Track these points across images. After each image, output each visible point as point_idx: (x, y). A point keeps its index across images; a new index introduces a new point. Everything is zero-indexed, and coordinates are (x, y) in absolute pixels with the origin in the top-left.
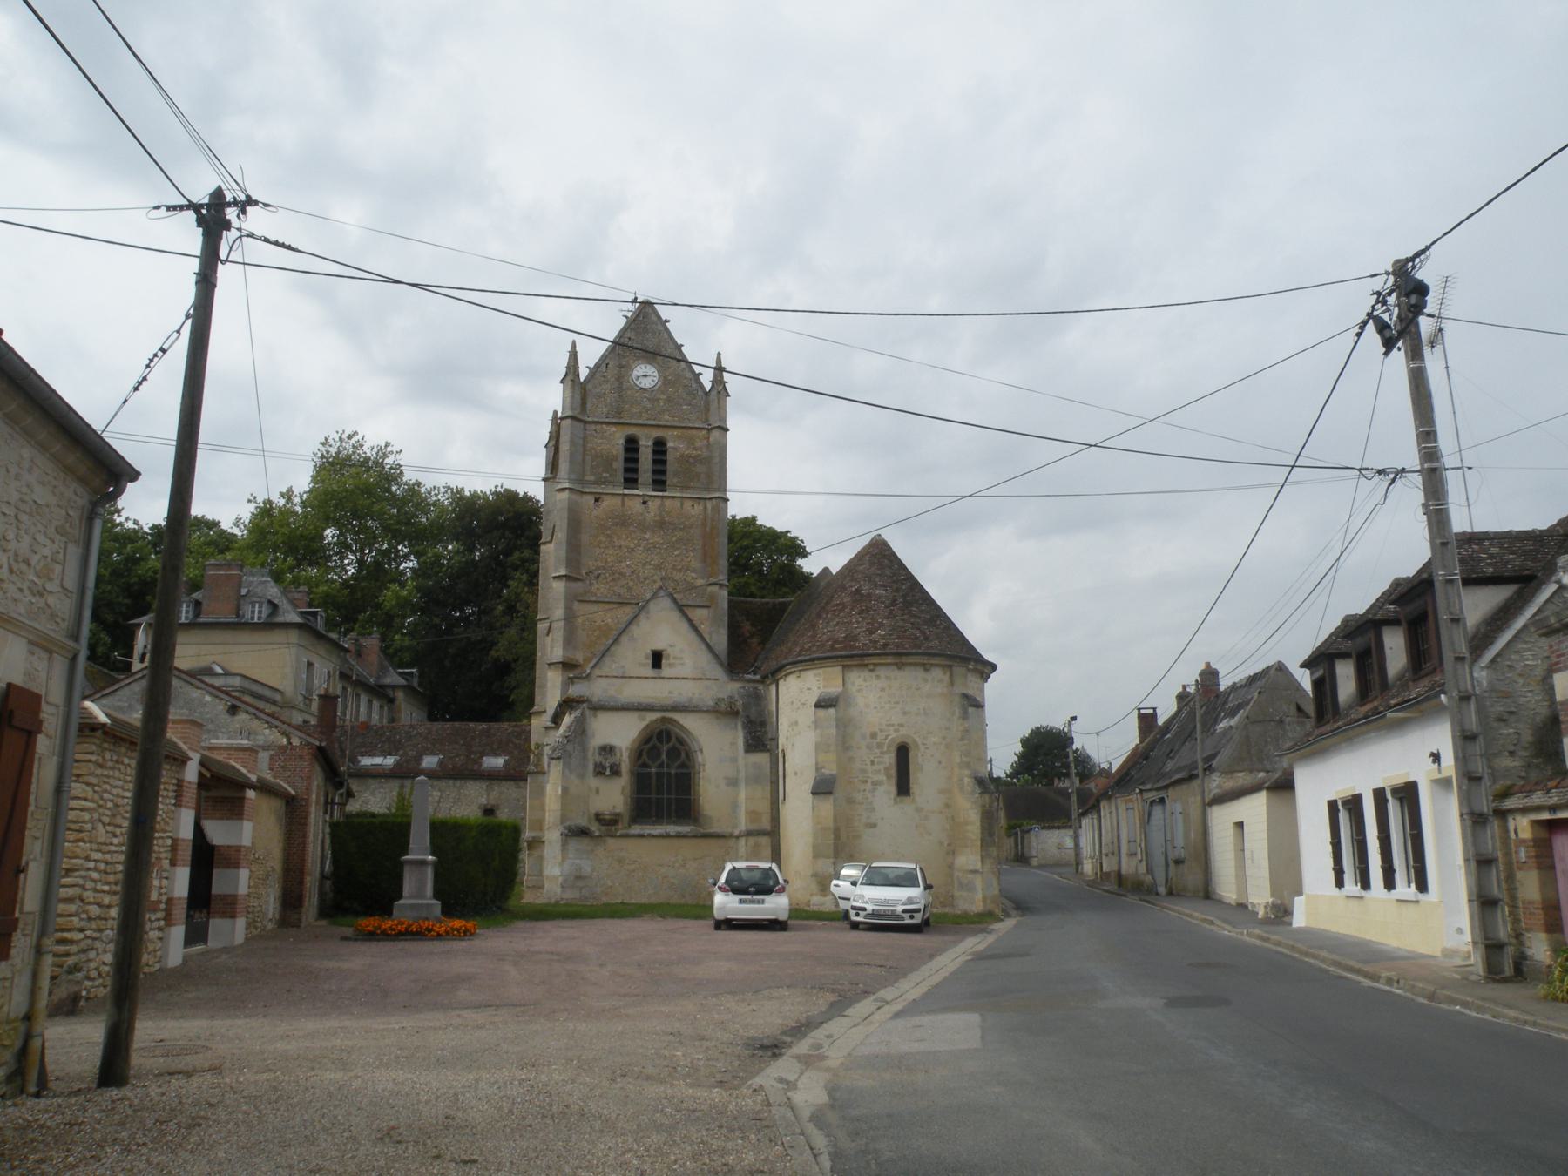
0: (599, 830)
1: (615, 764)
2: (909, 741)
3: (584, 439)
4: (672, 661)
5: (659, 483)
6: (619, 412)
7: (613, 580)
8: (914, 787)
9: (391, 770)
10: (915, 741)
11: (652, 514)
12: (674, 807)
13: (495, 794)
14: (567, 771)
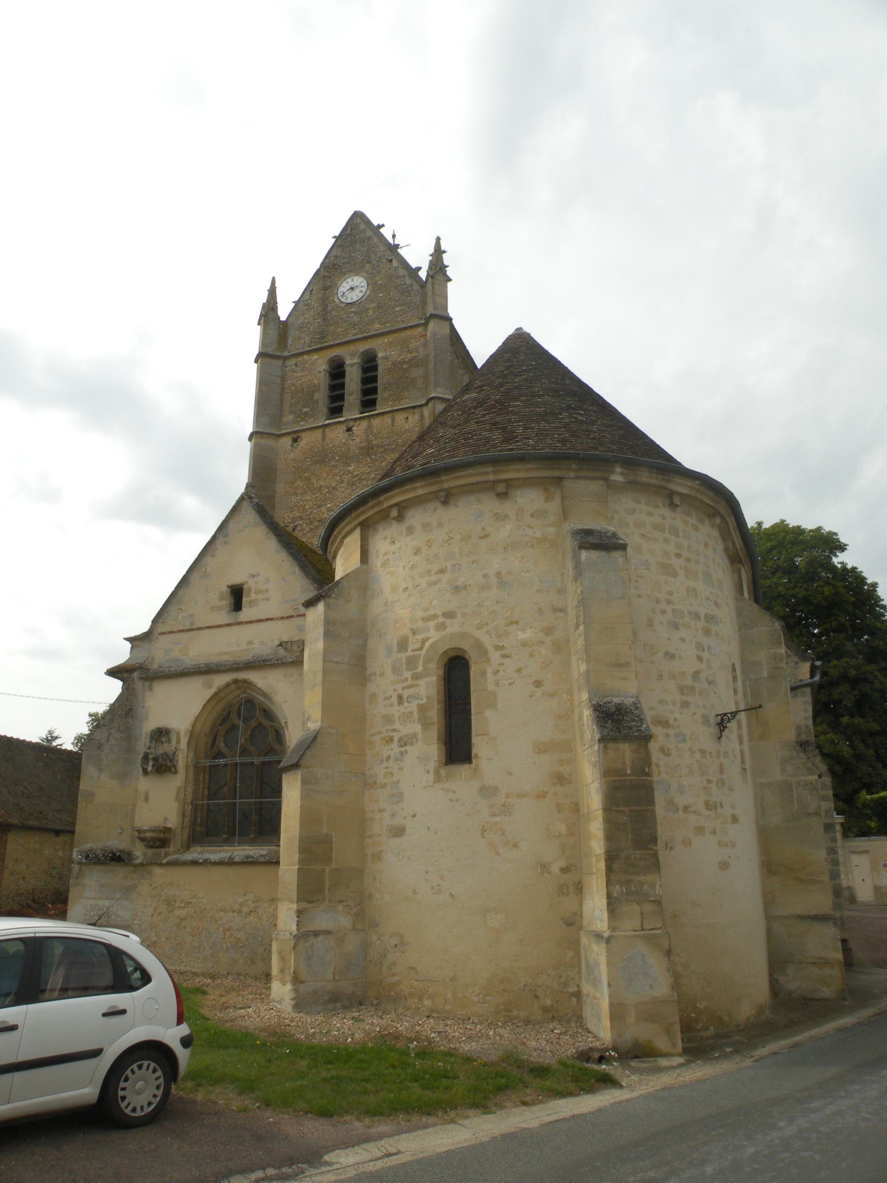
2: (465, 645)
5: (368, 402)
7: (311, 530)
8: (479, 745)
10: (479, 645)
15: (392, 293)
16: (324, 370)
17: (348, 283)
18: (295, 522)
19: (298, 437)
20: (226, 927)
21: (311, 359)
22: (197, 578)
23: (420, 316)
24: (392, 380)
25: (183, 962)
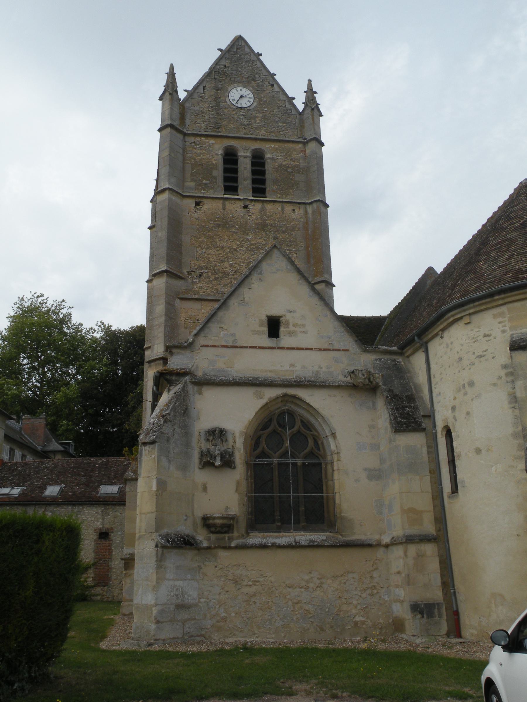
0: (209, 539)
1: (226, 452)
3: (184, 149)
4: (291, 328)
6: (217, 127)
9: (16, 498)
11: (254, 217)
12: (302, 509)
13: (109, 518)
14: (164, 459)
15: (275, 111)
16: (221, 154)
17: (241, 90)
18: (201, 270)
19: (200, 202)
20: (295, 601)
21: (208, 142)
22: (236, 304)
23: (299, 136)
24: (279, 178)
25: (255, 634)
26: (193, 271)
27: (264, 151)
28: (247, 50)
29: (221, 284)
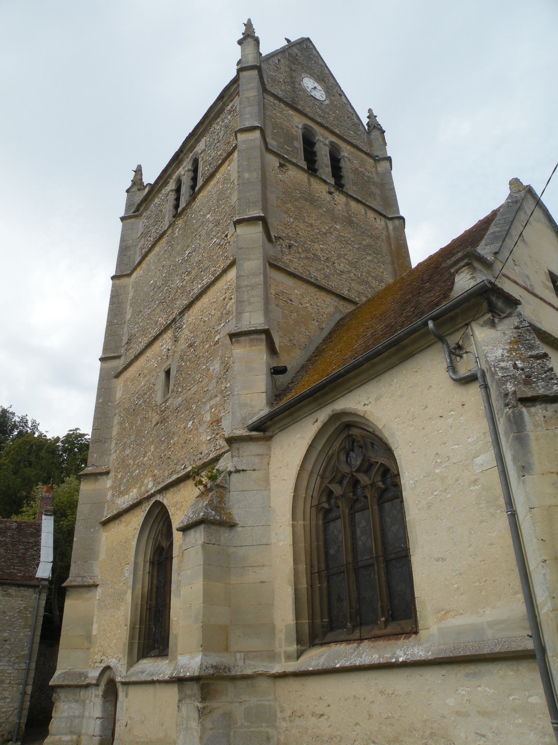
26: (281, 239)
27: (341, 148)
28: (314, 52)
29: (313, 267)
